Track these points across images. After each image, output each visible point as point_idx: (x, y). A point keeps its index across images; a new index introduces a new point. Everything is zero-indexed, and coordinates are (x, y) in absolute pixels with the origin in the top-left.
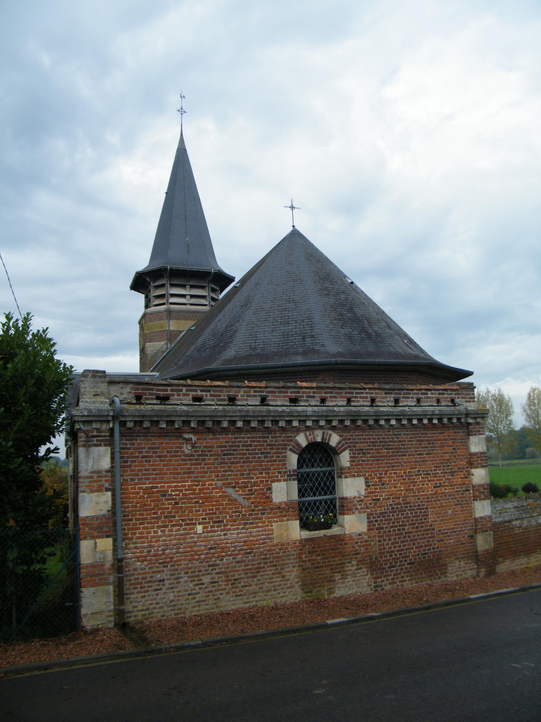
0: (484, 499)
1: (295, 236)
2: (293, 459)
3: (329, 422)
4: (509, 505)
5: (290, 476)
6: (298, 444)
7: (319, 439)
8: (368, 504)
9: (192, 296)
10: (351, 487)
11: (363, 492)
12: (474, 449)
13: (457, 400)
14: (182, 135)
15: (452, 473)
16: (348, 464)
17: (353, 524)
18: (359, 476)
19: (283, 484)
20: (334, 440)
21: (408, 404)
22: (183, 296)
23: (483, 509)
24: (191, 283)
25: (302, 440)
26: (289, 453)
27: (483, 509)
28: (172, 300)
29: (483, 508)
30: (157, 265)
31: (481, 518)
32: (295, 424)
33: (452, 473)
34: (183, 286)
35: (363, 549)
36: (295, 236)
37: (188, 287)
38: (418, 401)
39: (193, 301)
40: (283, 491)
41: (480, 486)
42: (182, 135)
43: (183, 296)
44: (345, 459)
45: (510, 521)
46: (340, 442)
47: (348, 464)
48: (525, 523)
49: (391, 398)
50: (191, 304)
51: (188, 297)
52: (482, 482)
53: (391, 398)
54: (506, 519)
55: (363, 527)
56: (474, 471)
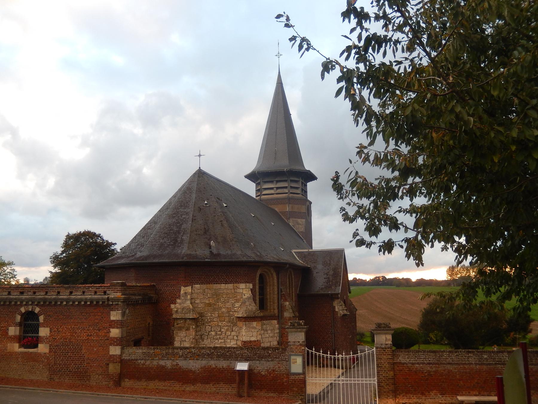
0: (117, 345)
1: (200, 174)
2: (18, 318)
3: (33, 302)
4: (140, 351)
5: (16, 325)
6: (21, 311)
7: (30, 310)
8: (50, 340)
9: (277, 188)
10: (44, 332)
11: (48, 335)
12: (112, 318)
13: (108, 292)
14: (279, 72)
15: (99, 330)
16: (42, 321)
17: (43, 348)
18: (47, 327)
19: (13, 328)
20: (37, 310)
21: (77, 295)
22: (272, 188)
23: (115, 351)
24: (276, 179)
25: (23, 310)
26: (17, 315)
27: (115, 351)
28: (264, 192)
29: (116, 350)
30: (264, 169)
31: (113, 355)
32: (19, 303)
33: (99, 330)
34: (272, 182)
35: (46, 361)
36: (200, 174)
37: (275, 182)
38: (84, 292)
39: (279, 191)
40: (13, 331)
41: (114, 338)
42: (279, 72)
43: (272, 188)
44: (41, 318)
45: (137, 360)
46: (39, 311)
47: (42, 321)
48: (148, 363)
49: (68, 291)
50: (277, 194)
51: (275, 189)
52: (117, 336)
53: (68, 291)
54: (133, 358)
55: (47, 350)
56: (111, 330)
